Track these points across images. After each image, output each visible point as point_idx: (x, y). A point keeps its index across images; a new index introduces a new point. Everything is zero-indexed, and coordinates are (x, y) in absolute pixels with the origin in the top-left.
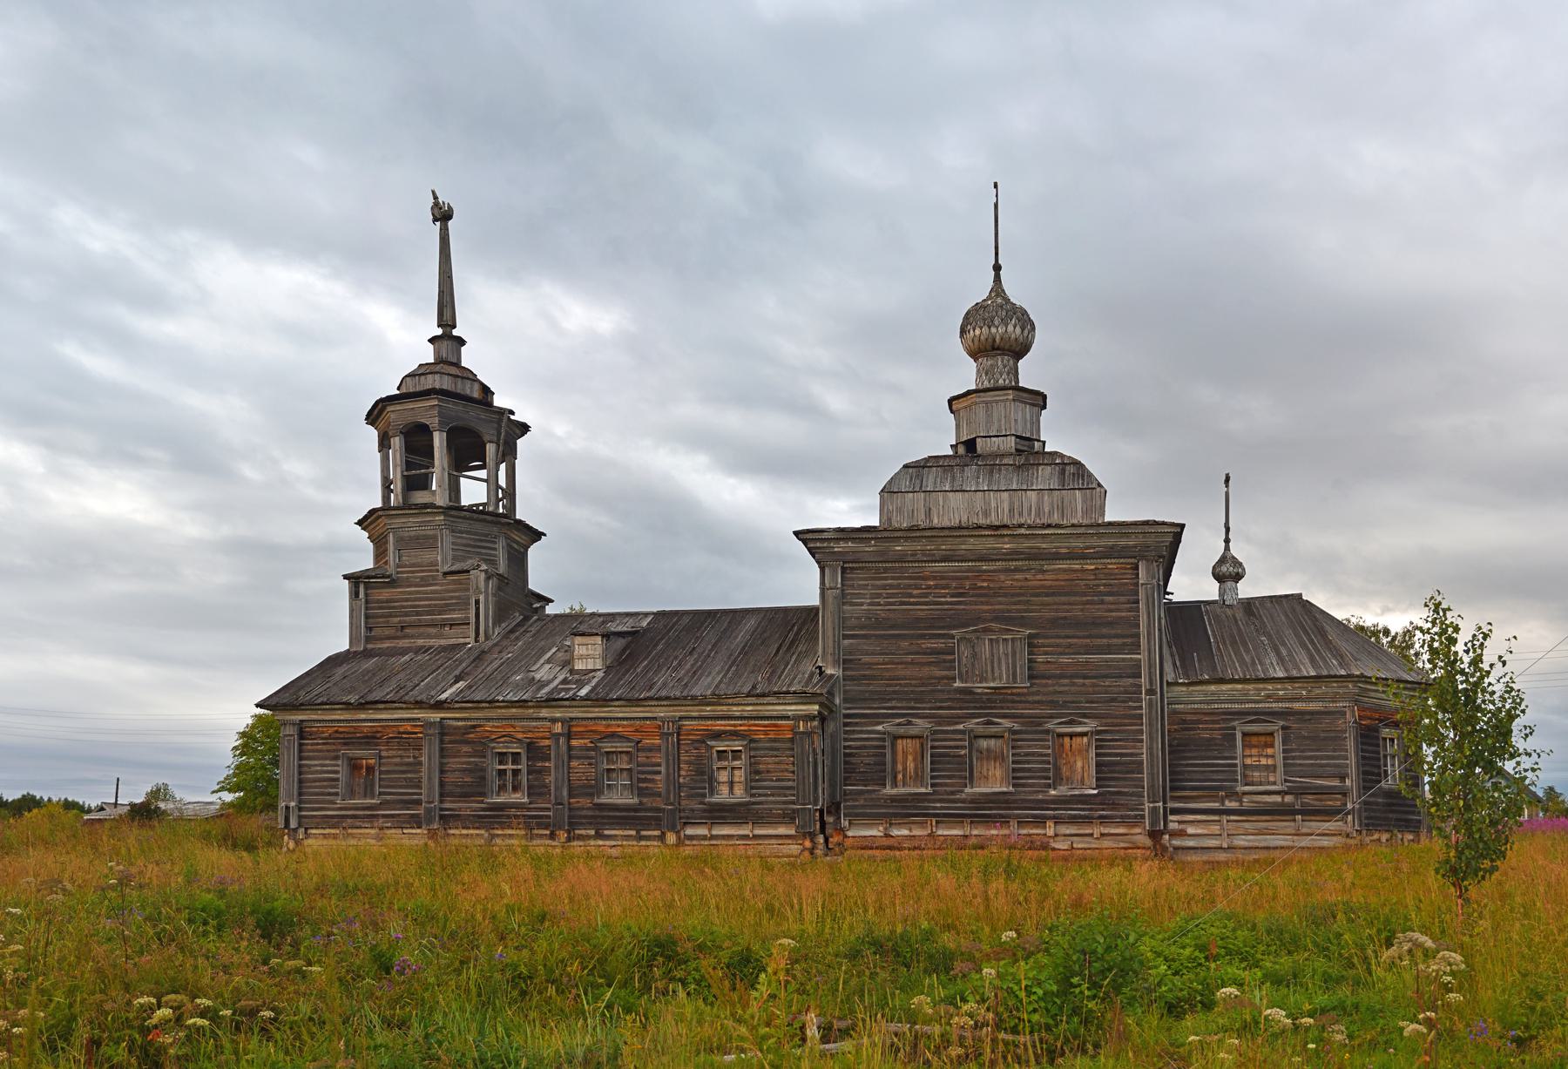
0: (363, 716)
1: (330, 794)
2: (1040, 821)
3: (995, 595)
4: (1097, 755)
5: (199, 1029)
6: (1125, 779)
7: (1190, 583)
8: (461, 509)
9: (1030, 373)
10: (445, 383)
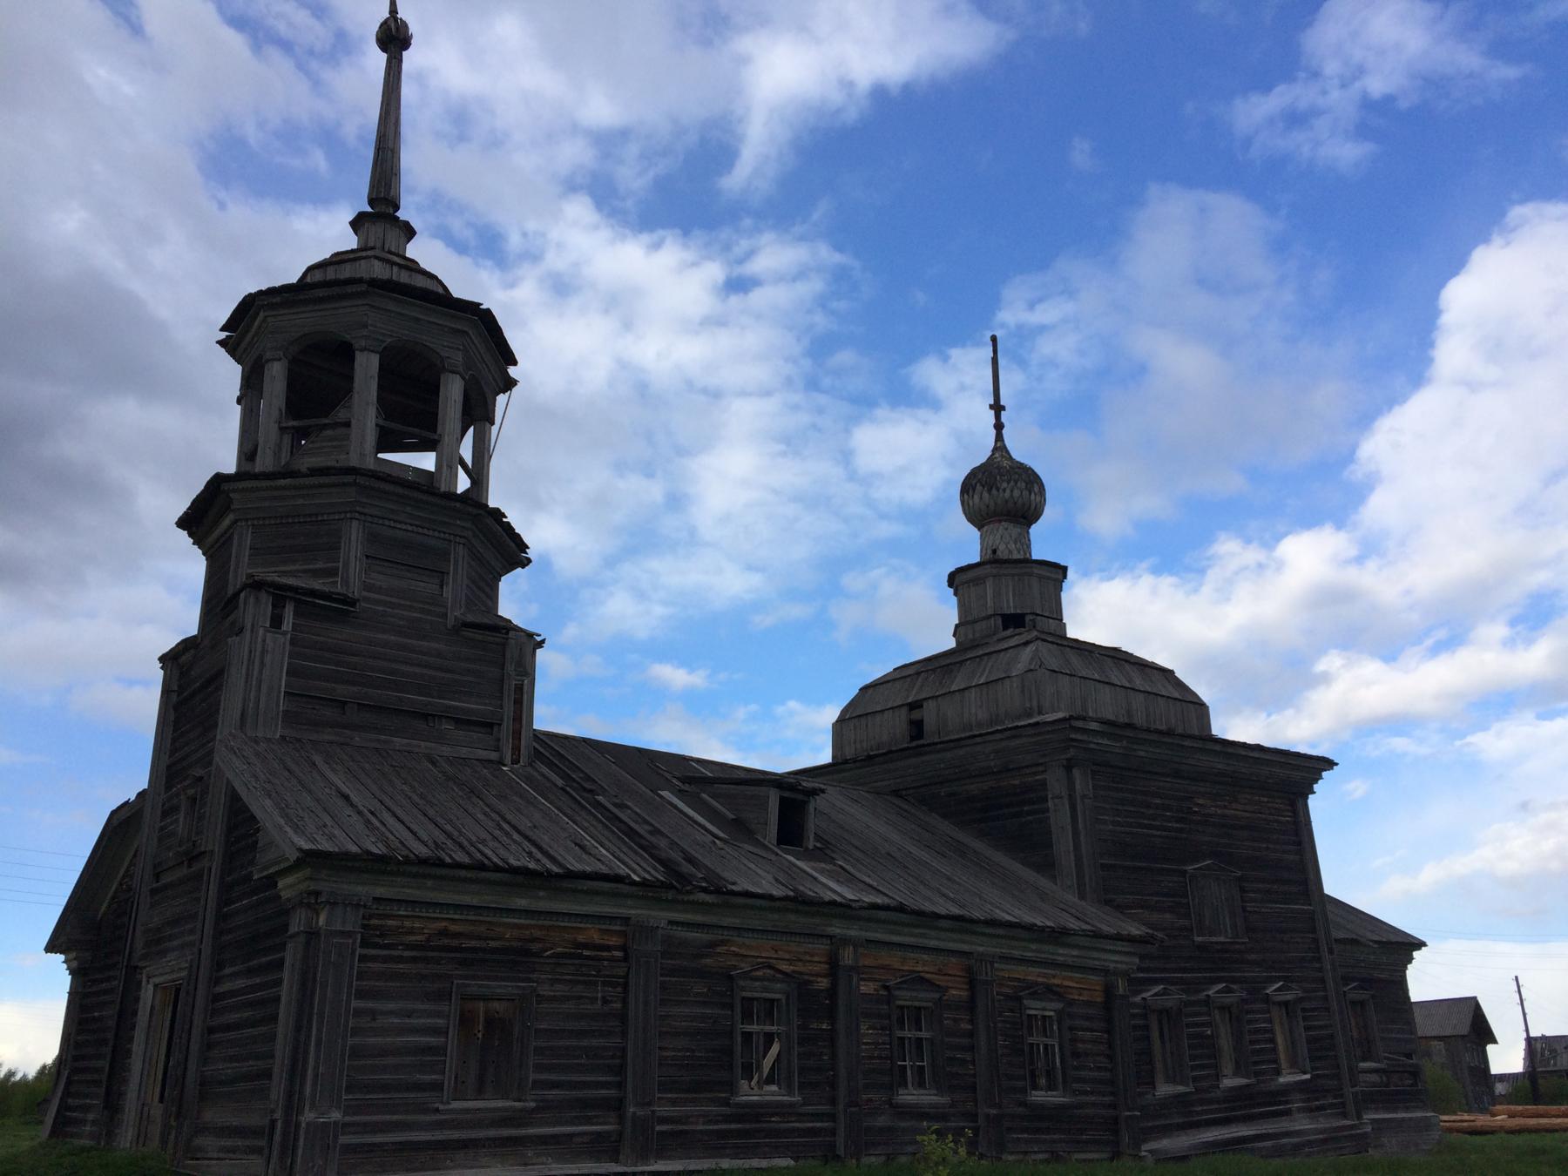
0: (522, 903)
1: (419, 1087)
2: (298, 1125)
3: (1325, 1141)
4: (1307, 1029)
5: (1364, 1060)
6: (636, 853)
7: (1506, 1058)
8: (1029, 561)
9: (1043, 542)
10: (379, 270)
